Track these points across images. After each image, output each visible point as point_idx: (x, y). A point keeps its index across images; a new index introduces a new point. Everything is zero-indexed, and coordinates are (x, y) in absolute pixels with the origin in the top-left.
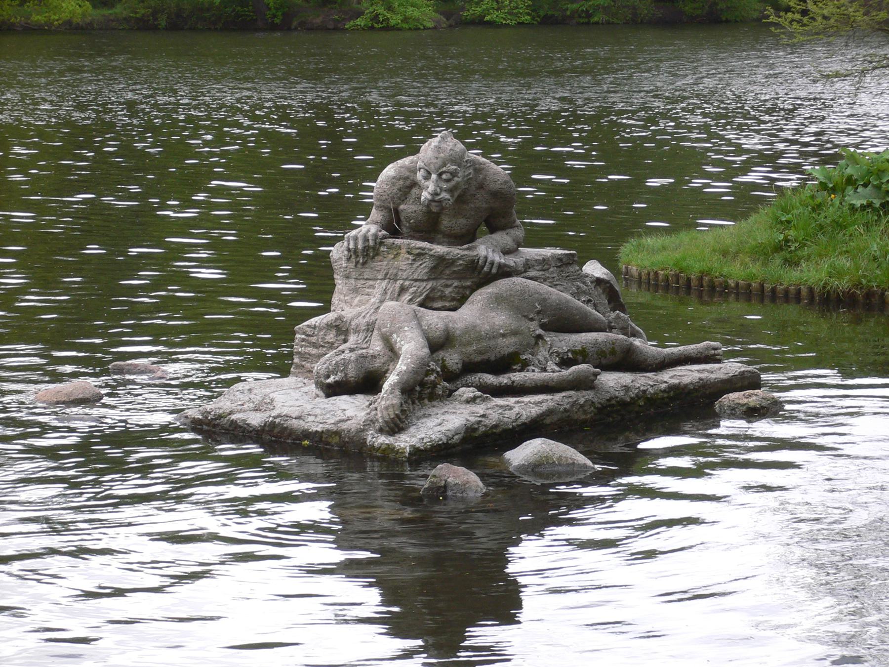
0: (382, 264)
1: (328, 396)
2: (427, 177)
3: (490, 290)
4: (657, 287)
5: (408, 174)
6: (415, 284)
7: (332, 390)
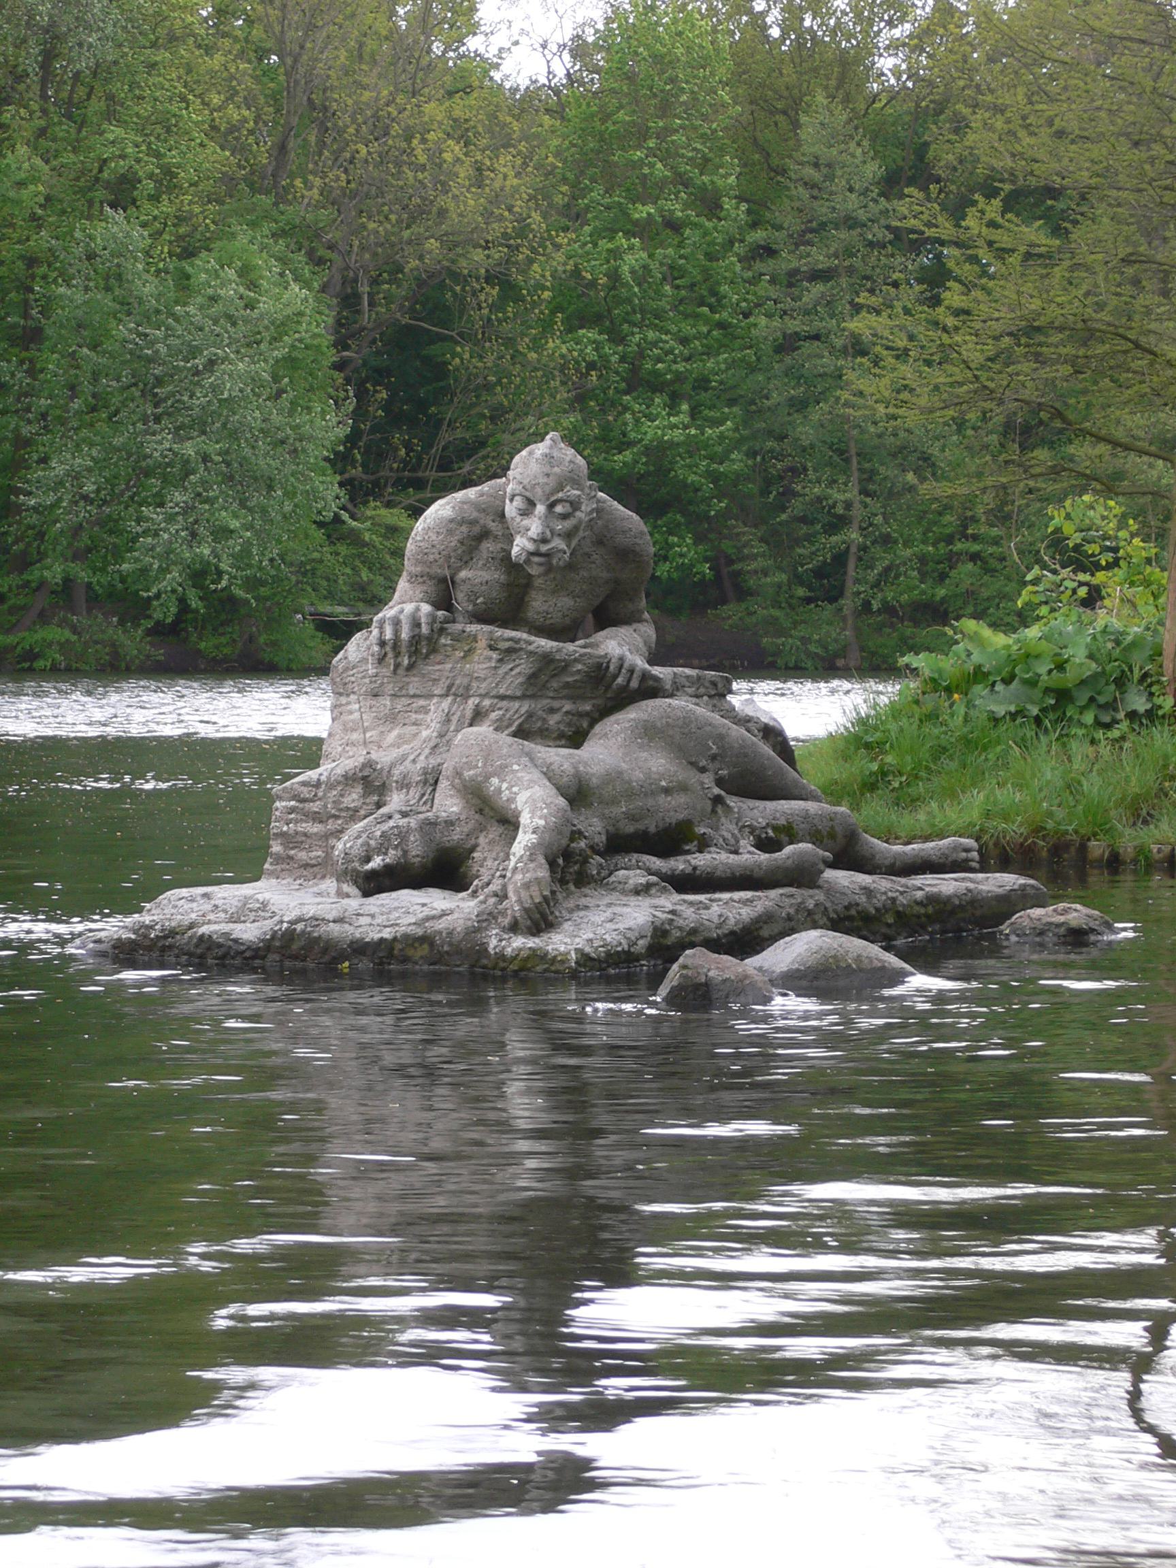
0: (442, 669)
1: (367, 894)
2: (526, 512)
3: (632, 715)
4: (437, 980)
5: (475, 514)
6: (504, 703)
7: (375, 883)
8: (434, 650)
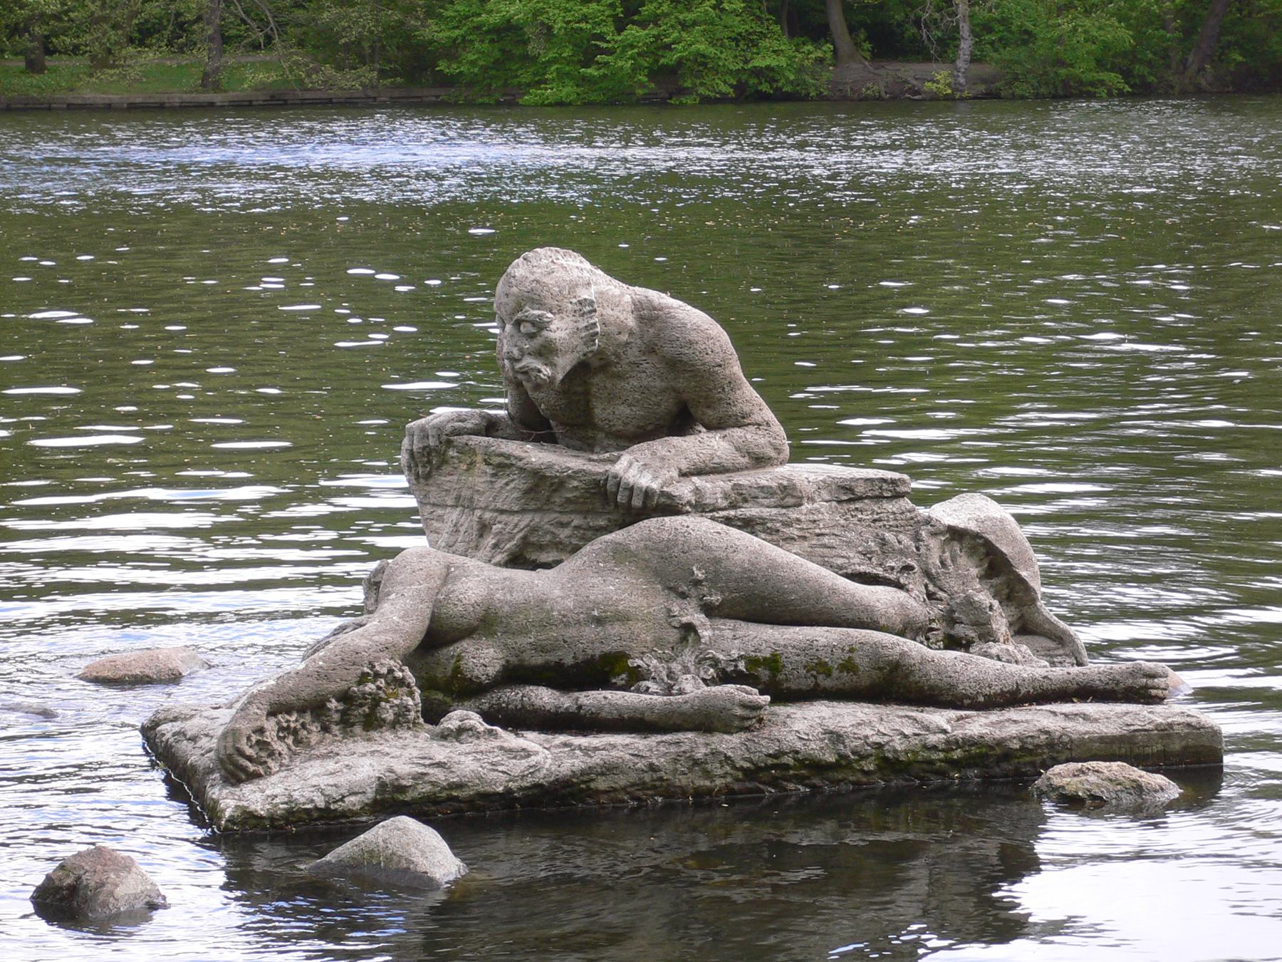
6: (504, 517)
8: (444, 462)
